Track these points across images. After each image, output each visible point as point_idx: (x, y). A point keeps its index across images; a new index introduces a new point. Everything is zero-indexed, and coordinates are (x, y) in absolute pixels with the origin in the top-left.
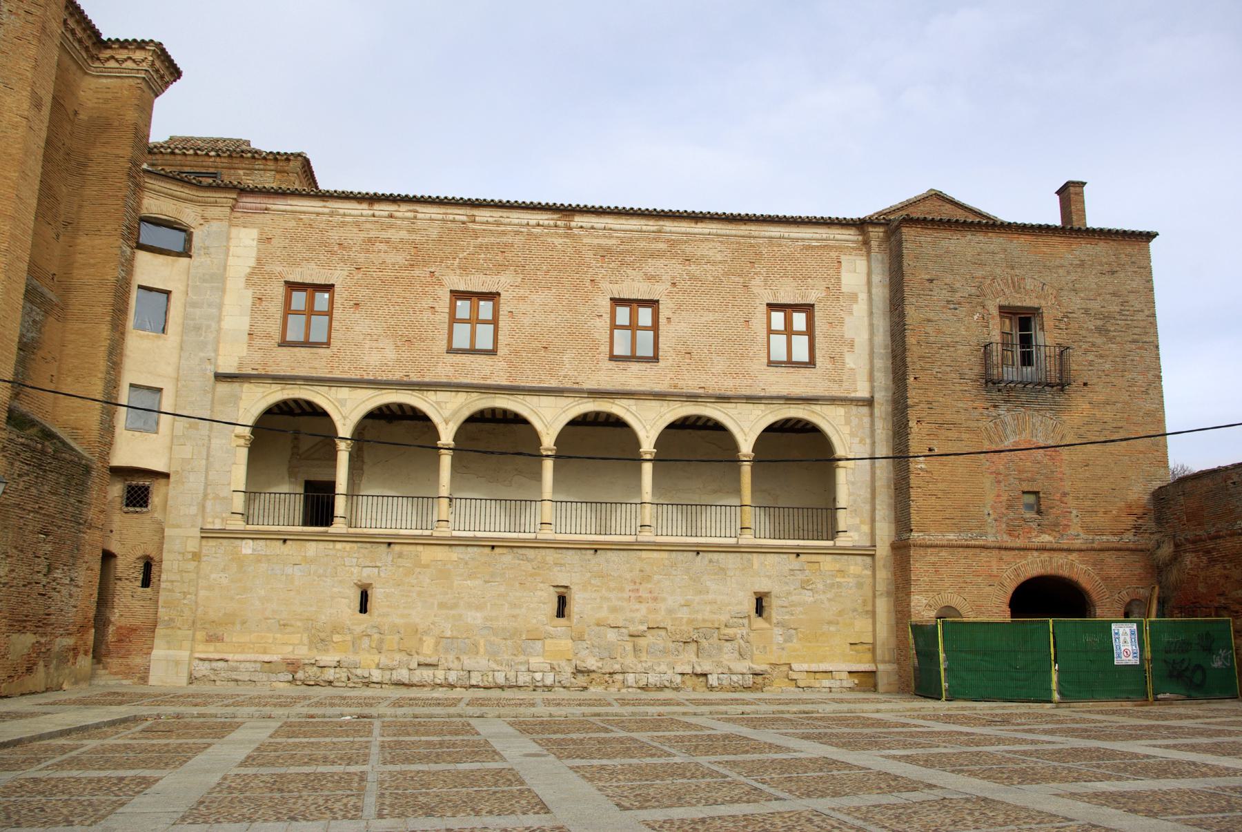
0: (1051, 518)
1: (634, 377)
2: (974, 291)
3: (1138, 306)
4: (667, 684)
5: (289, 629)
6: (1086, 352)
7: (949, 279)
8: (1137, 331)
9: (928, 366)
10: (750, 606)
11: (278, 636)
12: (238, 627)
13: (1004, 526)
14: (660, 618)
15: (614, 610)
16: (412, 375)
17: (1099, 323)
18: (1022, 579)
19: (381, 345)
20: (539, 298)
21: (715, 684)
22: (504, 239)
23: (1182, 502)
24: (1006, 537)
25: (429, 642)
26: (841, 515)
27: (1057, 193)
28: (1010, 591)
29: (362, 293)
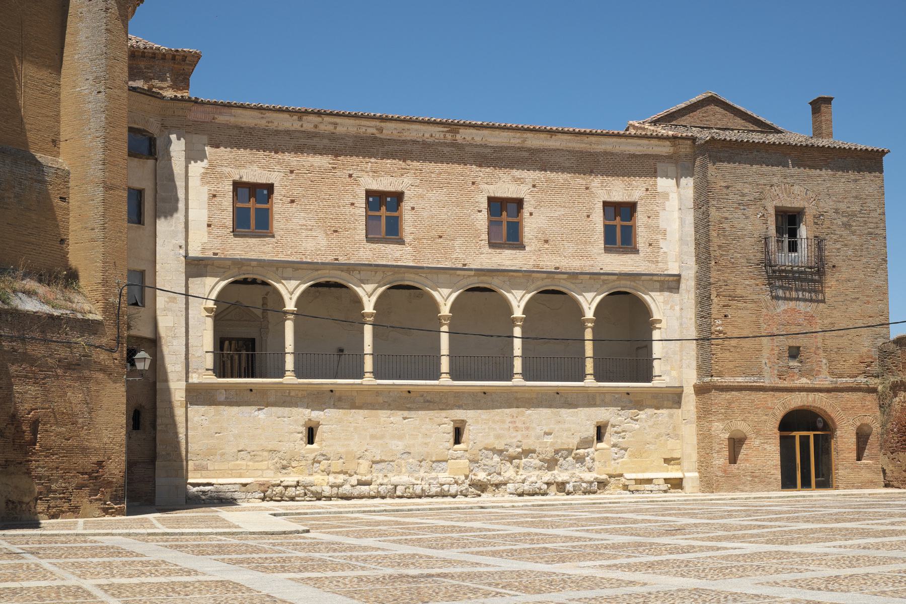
0: (808, 366)
1: (507, 259)
2: (757, 195)
3: (873, 206)
4: (538, 491)
5: (258, 458)
6: (836, 241)
7: (739, 186)
8: (872, 225)
9: (724, 253)
10: (593, 432)
11: (250, 463)
12: (218, 457)
13: (776, 372)
14: (528, 444)
15: (498, 437)
16: (340, 258)
17: (845, 219)
18: (787, 410)
19: (314, 234)
20: (435, 195)
21: (571, 489)
22: (405, 147)
23: (899, 355)
24: (777, 380)
25: (364, 465)
26: (656, 363)
27: (810, 103)
28: (780, 418)
29: (297, 192)
